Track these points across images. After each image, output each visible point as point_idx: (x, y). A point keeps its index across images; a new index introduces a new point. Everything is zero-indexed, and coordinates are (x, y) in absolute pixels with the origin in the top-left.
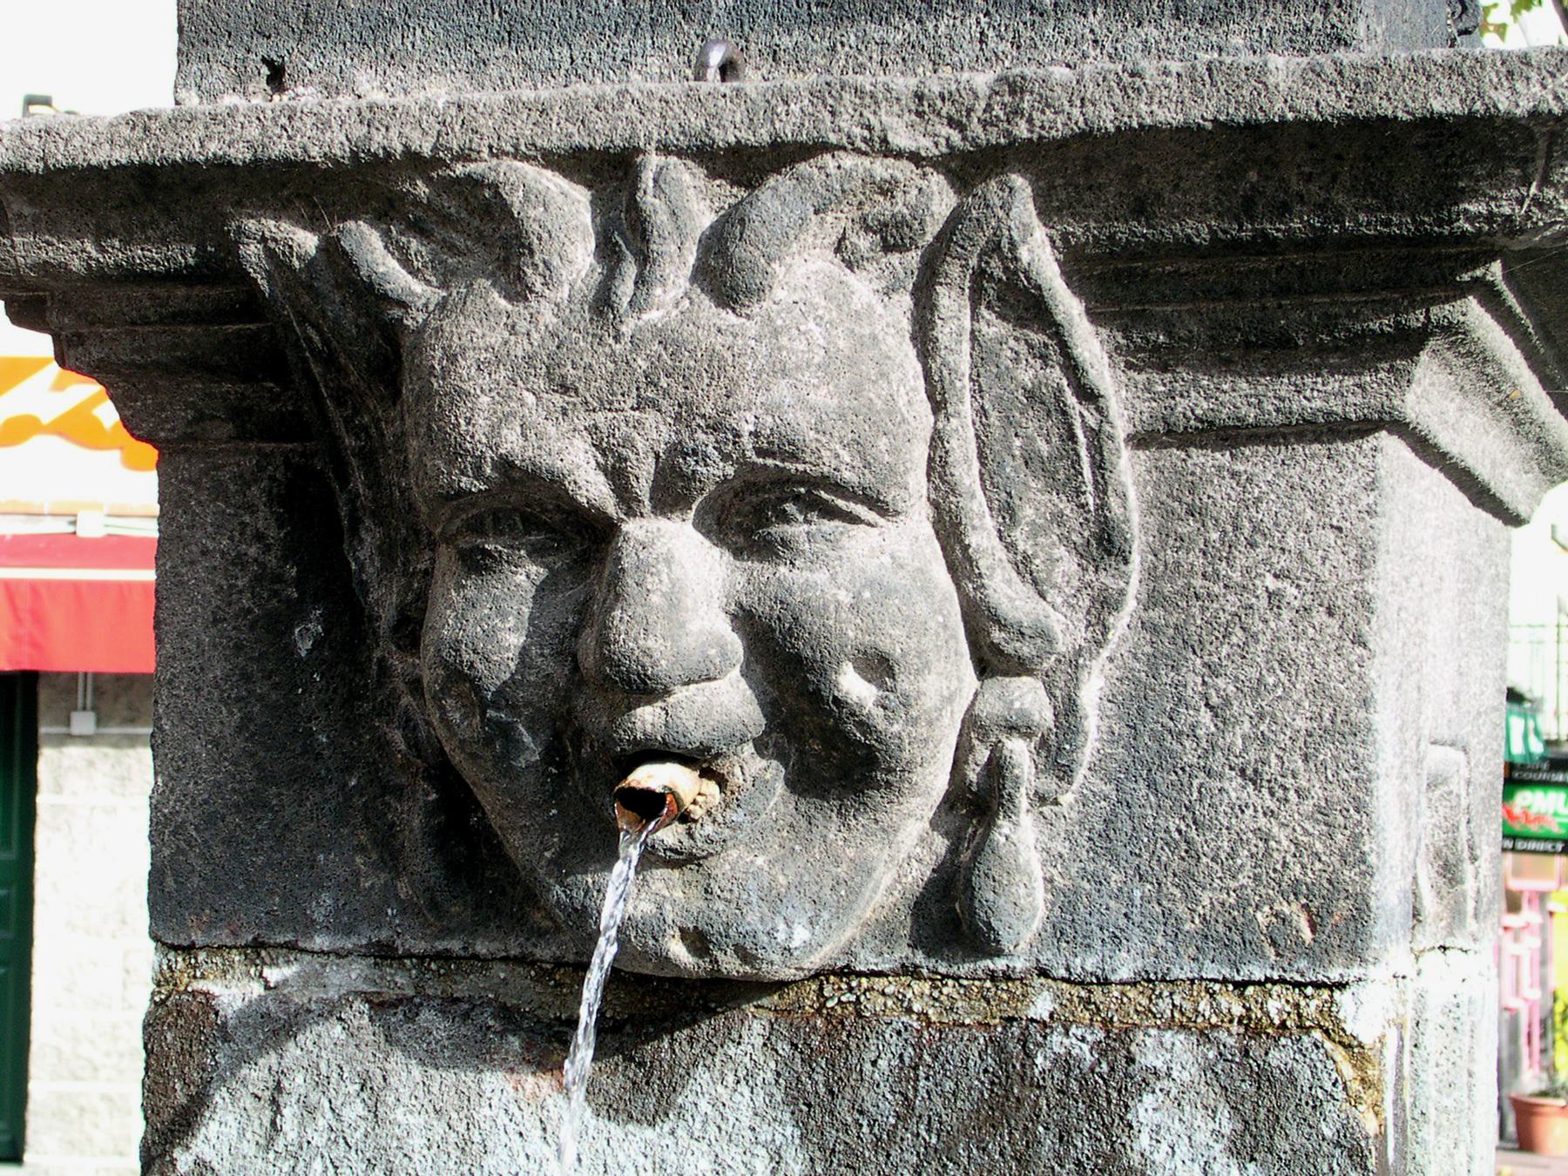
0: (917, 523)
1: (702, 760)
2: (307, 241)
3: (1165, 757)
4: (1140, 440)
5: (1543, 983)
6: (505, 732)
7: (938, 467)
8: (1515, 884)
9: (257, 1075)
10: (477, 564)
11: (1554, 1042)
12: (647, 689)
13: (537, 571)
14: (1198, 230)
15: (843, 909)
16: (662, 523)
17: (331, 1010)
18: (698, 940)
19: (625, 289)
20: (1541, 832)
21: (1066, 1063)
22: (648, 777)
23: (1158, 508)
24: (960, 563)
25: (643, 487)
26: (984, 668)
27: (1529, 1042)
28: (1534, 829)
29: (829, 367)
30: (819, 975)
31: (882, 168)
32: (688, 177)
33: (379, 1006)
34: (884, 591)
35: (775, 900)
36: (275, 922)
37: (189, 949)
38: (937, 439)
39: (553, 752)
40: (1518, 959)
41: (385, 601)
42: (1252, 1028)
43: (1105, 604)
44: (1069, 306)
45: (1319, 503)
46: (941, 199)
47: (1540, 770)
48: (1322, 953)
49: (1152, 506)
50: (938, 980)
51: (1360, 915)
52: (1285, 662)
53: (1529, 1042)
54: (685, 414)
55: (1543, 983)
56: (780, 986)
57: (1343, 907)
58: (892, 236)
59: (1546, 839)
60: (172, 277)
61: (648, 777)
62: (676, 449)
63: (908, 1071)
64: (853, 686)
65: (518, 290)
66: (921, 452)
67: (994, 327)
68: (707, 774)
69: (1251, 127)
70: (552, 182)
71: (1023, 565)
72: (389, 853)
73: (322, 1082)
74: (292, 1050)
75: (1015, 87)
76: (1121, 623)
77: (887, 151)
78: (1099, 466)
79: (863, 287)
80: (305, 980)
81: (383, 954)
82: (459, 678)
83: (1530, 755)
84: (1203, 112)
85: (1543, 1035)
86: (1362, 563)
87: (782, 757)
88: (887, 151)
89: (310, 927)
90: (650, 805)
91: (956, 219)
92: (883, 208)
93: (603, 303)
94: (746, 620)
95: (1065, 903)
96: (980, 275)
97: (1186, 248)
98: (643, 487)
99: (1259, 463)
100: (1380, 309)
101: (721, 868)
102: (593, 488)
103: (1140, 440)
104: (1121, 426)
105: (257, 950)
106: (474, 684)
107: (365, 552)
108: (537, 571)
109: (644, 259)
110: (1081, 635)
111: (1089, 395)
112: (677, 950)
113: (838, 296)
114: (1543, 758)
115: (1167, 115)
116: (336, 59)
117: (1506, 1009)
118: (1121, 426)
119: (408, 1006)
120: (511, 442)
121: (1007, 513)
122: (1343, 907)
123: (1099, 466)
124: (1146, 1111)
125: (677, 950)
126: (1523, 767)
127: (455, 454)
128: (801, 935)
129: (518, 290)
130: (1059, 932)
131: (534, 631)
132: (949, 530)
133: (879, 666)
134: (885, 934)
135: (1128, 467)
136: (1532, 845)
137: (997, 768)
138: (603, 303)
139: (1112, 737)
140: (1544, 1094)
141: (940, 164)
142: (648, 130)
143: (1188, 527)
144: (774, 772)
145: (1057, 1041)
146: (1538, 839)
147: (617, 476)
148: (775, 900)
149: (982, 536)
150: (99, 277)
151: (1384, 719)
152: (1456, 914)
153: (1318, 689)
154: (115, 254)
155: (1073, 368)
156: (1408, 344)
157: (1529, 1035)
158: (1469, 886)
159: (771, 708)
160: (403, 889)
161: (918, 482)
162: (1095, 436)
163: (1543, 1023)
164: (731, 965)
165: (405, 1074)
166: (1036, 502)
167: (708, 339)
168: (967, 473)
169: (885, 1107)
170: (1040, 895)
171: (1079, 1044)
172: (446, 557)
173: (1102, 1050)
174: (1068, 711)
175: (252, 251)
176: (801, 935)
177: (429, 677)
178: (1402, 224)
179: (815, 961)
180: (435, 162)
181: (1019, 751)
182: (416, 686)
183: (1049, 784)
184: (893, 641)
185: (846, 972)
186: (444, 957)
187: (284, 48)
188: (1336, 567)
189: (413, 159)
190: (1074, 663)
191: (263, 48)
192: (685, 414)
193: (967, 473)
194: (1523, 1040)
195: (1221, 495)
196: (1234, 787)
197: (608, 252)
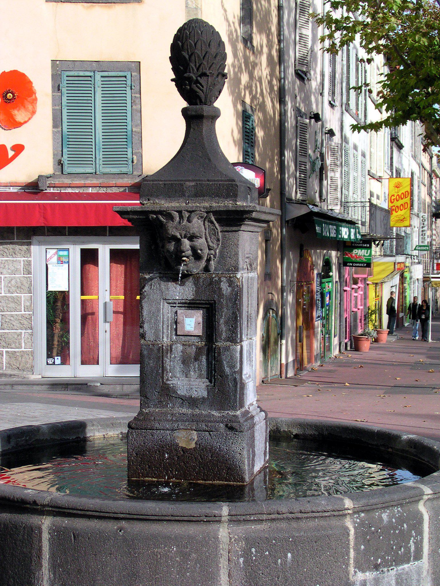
0: (204, 239)
1: (188, 257)
2: (155, 216)
3: (223, 256)
4: (221, 232)
5: (365, 304)
6: (172, 255)
7: (205, 235)
8: (355, 276)
9: (149, 283)
10: (170, 242)
11: (368, 321)
12: (184, 252)
13: (174, 243)
14: (224, 217)
15: (198, 269)
16: (185, 239)
17: (156, 278)
18: (187, 271)
19: (182, 221)
20: (360, 261)
21: (216, 280)
22: (184, 258)
23: (223, 237)
24: (207, 242)
25: (183, 236)
26: (209, 250)
27: (361, 322)
28: (358, 260)
29: (197, 228)
30: (196, 274)
31: (201, 212)
32: (186, 213)
33: (160, 277)
34: (201, 244)
35: (193, 268)
36: (151, 271)
37: (143, 273)
38: (205, 232)
39: (175, 257)
40: (356, 297)
41: (160, 245)
42: (230, 277)
43: (218, 245)
44: (215, 222)
45: (235, 237)
46: (206, 215)
47: (360, 243)
48: (235, 271)
49: (222, 237)
50: (205, 274)
51: (238, 268)
52: (232, 249)
53: (361, 322)
54: (186, 231)
55: (365, 304)
56: (193, 275)
57: (237, 268)
58: (202, 217)
59: (362, 263)
60: (142, 219)
61: (184, 258)
62: (186, 234)
63: (203, 281)
64: (199, 251)
65: (173, 221)
66: (204, 233)
67: (209, 224)
68: (188, 258)
69: (228, 210)
70: (175, 213)
71: (212, 242)
72: (160, 265)
73: (155, 284)
74: (153, 281)
75: (211, 207)
76: (220, 246)
77: (201, 211)
78: (218, 234)
79: (199, 221)
80: (153, 275)
81: (160, 273)
82: (168, 251)
83: (357, 239)
84: (225, 209)
85: (365, 320)
86: (238, 241)
87: (194, 257)
88: (201, 211)
89: (154, 271)
90: (184, 261)
91: (207, 216)
92: (201, 215)
93: (180, 222)
94: (191, 246)
95: (215, 268)
96: (208, 220)
97: (224, 218)
98: (183, 236)
99: (230, 234)
100: (239, 222)
101: (189, 265)
102: (179, 237)
103: (221, 232)
104: (219, 231)
105: (149, 273)
106: (170, 252)
107: (158, 241)
108: (174, 243)
109: (183, 219)
110: (217, 247)
111: (217, 229)
112: (185, 272)
113: (198, 222)
114: (361, 240)
115: (222, 209)
116: (154, 199)
117: (352, 311)
118: (219, 231)
119: (162, 277)
120: (173, 233)
121: (211, 238)
122: (237, 268)
123: (218, 234)
124: (222, 283)
125: (185, 272)
126: (355, 243)
127: (168, 234)
128: (195, 270)
129: (173, 221)
130: (215, 270)
131: (174, 248)
132: (206, 239)
133: (201, 250)
134: (201, 271)
135: (220, 234)
136: (358, 265)
137: (210, 257)
138: (180, 222)
139: (219, 255)
140: (362, 335)
141: (205, 212)
142: (183, 209)
143: (225, 238)
144: (193, 258)
145: (215, 279)
146: (360, 263)
147: (181, 236)
148: (193, 268)
149: (209, 240)
150: (137, 219)
151: (240, 254)
152: (252, 270)
153: (235, 251)
154: (138, 217)
155: (216, 227)
156: (241, 225)
157: (361, 319)
158: (253, 267)
159: (193, 253)
160: (162, 268)
161: (204, 236)
162: (217, 232)
163: (365, 316)
164: (190, 273)
165: (162, 283)
166: (213, 237)
167: (188, 225)
168: (208, 235)
169: (202, 284)
170: (214, 267)
171: (217, 279)
172: (166, 241)
173: (218, 279)
174: (216, 253)
175: (150, 217)
176: (195, 270)
177: (165, 251)
178: (239, 217)
179: (196, 273)
180: (166, 211)
181: (212, 256)
182: (164, 252)
183: (214, 259)
184: (202, 248)
185: (198, 274)
186: (166, 273)
187: (149, 198)
188: (236, 242)
189: (164, 211)
190: (216, 249)
191: (147, 197)
192: (186, 231)
193: (208, 235)
194: (358, 321)
195: (227, 236)
196: (228, 258)
197: (180, 218)
